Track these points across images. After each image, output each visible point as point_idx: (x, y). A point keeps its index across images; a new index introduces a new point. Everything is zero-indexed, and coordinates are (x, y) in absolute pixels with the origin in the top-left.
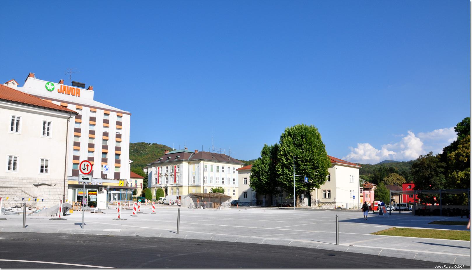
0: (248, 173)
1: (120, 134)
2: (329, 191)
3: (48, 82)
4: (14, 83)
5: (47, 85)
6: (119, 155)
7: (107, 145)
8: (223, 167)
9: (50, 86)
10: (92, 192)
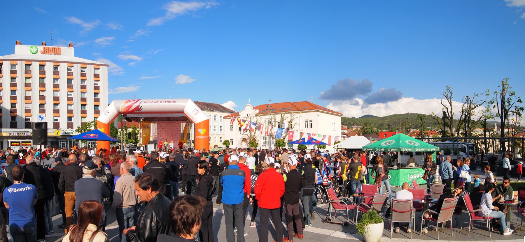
1: (99, 85)
2: (311, 121)
3: (32, 46)
6: (85, 105)
8: (209, 115)
9: (34, 49)
10: (26, 143)
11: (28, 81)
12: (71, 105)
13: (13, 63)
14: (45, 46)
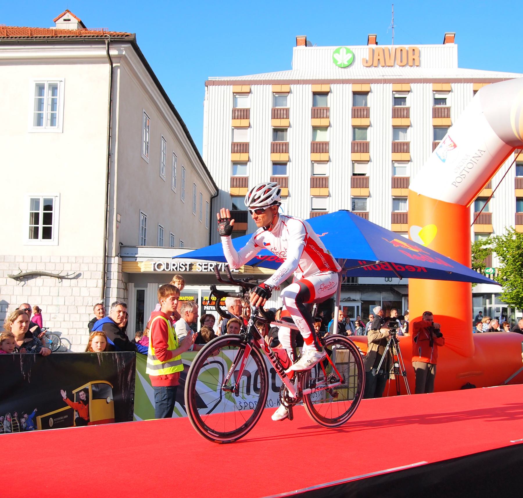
0: (208, 286)
4: (69, 20)
5: (336, 56)
7: (287, 141)
11: (321, 137)
13: (279, 91)
14: (374, 46)
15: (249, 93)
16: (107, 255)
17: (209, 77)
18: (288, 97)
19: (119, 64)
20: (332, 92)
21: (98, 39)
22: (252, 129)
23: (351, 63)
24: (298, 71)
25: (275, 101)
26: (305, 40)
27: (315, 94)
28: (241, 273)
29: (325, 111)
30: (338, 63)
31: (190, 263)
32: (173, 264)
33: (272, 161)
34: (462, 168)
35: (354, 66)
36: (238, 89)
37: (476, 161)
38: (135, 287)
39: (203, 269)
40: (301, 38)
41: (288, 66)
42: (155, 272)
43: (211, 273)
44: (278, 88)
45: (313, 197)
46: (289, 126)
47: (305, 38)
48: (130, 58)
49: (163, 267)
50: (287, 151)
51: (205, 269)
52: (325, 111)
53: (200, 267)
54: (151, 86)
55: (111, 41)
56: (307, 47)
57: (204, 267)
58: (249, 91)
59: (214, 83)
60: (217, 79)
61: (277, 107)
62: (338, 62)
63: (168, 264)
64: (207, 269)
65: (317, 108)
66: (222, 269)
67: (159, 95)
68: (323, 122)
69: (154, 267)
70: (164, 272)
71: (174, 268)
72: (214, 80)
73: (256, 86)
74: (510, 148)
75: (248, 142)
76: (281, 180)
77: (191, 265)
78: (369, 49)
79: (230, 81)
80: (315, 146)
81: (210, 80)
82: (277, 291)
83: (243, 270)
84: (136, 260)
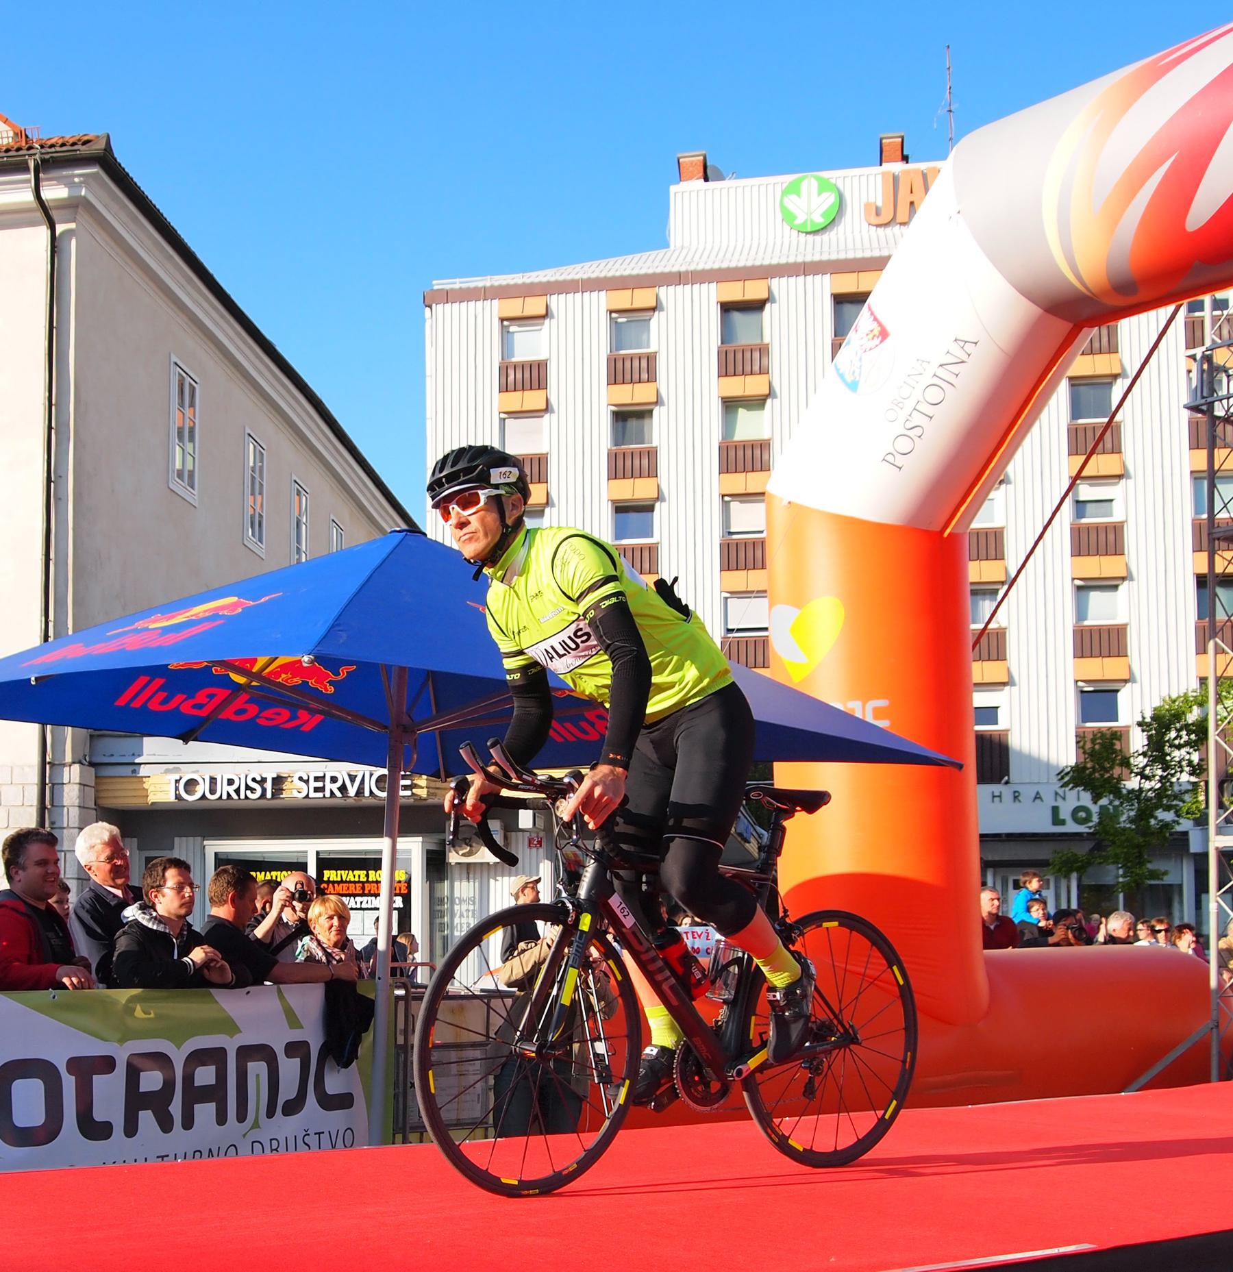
5: (791, 202)
7: (654, 445)
11: (749, 426)
12: (1110, 585)
13: (627, 306)
14: (897, 167)
15: (544, 317)
16: (48, 760)
17: (434, 282)
18: (654, 323)
19: (73, 226)
20: (774, 301)
21: (7, 157)
22: (554, 416)
23: (834, 219)
24: (684, 252)
25: (618, 334)
26: (702, 164)
27: (727, 308)
28: (421, 799)
29: (756, 355)
30: (798, 222)
31: (275, 776)
32: (229, 780)
33: (612, 501)
34: (910, 405)
35: (841, 228)
36: (514, 307)
37: (951, 378)
38: (140, 848)
39: (312, 790)
40: (692, 159)
41: (660, 241)
42: (181, 805)
43: (333, 802)
44: (623, 299)
45: (728, 595)
46: (656, 403)
47: (702, 158)
48: (105, 206)
49: (202, 788)
50: (652, 473)
51: (316, 790)
52: (756, 355)
53: (303, 785)
54: (189, 288)
55: (43, 161)
56: (710, 184)
57: (313, 784)
58: (543, 312)
59: (448, 297)
60: (457, 284)
61: (622, 352)
62: (795, 218)
63: (213, 780)
64: (322, 789)
65: (734, 348)
66: (363, 789)
67: (222, 316)
68: (752, 386)
69: (177, 788)
70: (204, 804)
71: (231, 789)
72: (448, 287)
73: (562, 297)
74: (1064, 327)
75: (544, 452)
76: (637, 554)
77: (278, 781)
78: (884, 174)
79: (492, 287)
80: (732, 453)
81: (437, 290)
82: (534, 850)
83: (425, 790)
84: (134, 771)
